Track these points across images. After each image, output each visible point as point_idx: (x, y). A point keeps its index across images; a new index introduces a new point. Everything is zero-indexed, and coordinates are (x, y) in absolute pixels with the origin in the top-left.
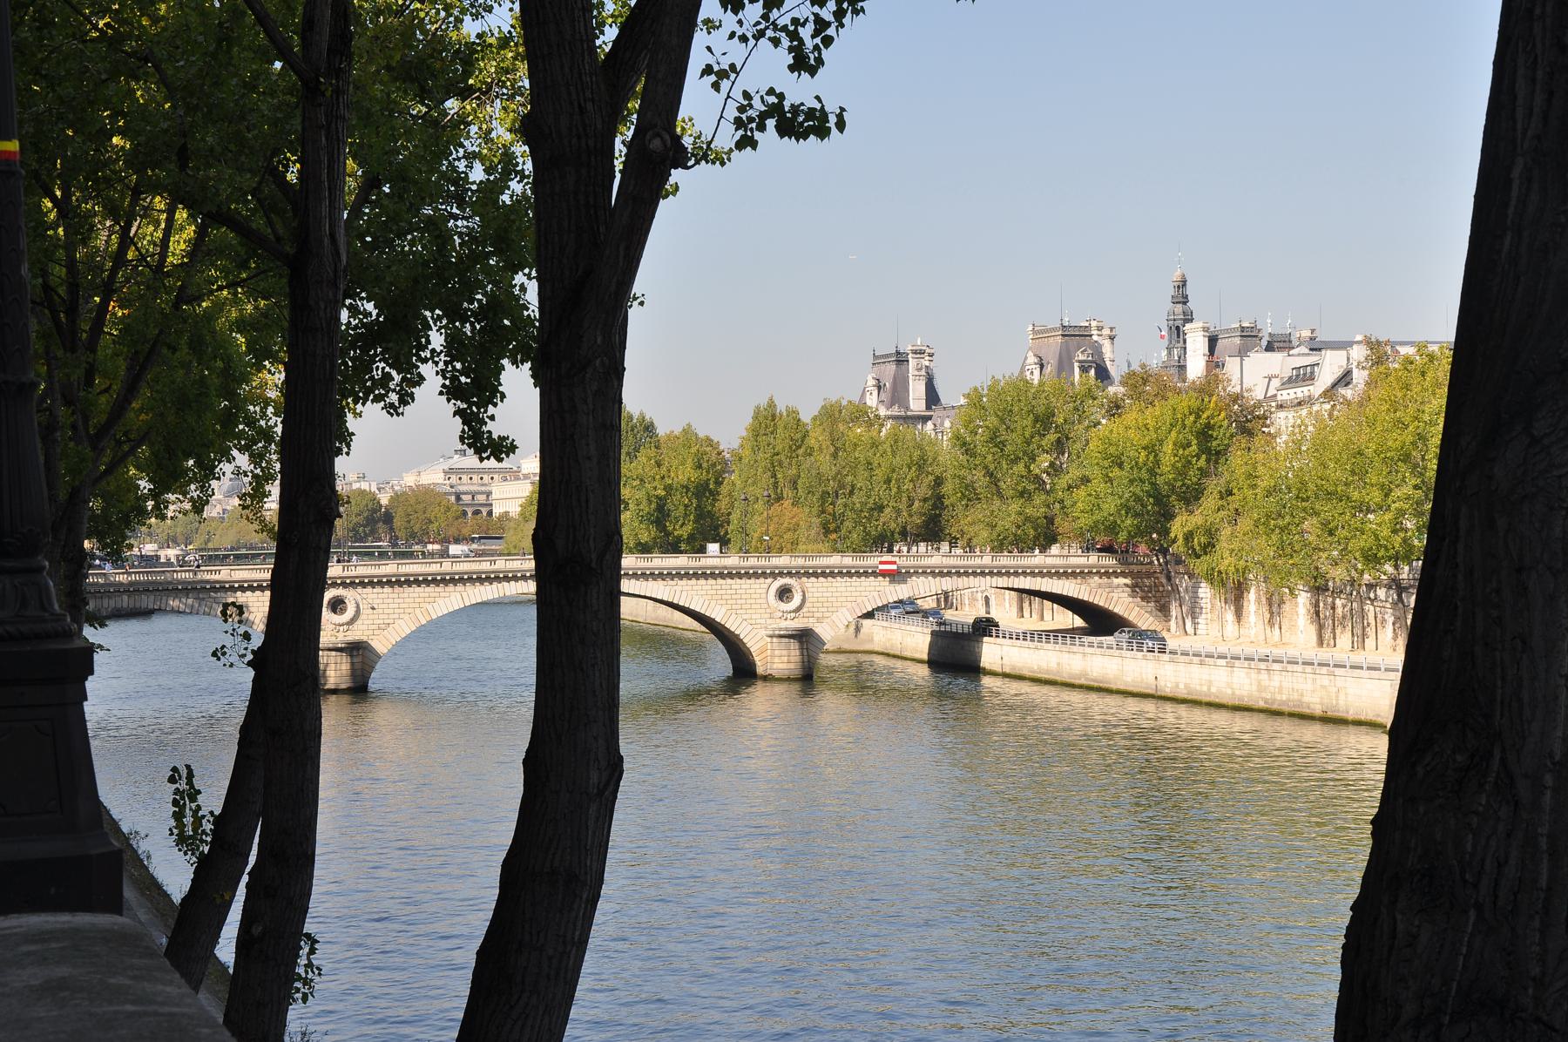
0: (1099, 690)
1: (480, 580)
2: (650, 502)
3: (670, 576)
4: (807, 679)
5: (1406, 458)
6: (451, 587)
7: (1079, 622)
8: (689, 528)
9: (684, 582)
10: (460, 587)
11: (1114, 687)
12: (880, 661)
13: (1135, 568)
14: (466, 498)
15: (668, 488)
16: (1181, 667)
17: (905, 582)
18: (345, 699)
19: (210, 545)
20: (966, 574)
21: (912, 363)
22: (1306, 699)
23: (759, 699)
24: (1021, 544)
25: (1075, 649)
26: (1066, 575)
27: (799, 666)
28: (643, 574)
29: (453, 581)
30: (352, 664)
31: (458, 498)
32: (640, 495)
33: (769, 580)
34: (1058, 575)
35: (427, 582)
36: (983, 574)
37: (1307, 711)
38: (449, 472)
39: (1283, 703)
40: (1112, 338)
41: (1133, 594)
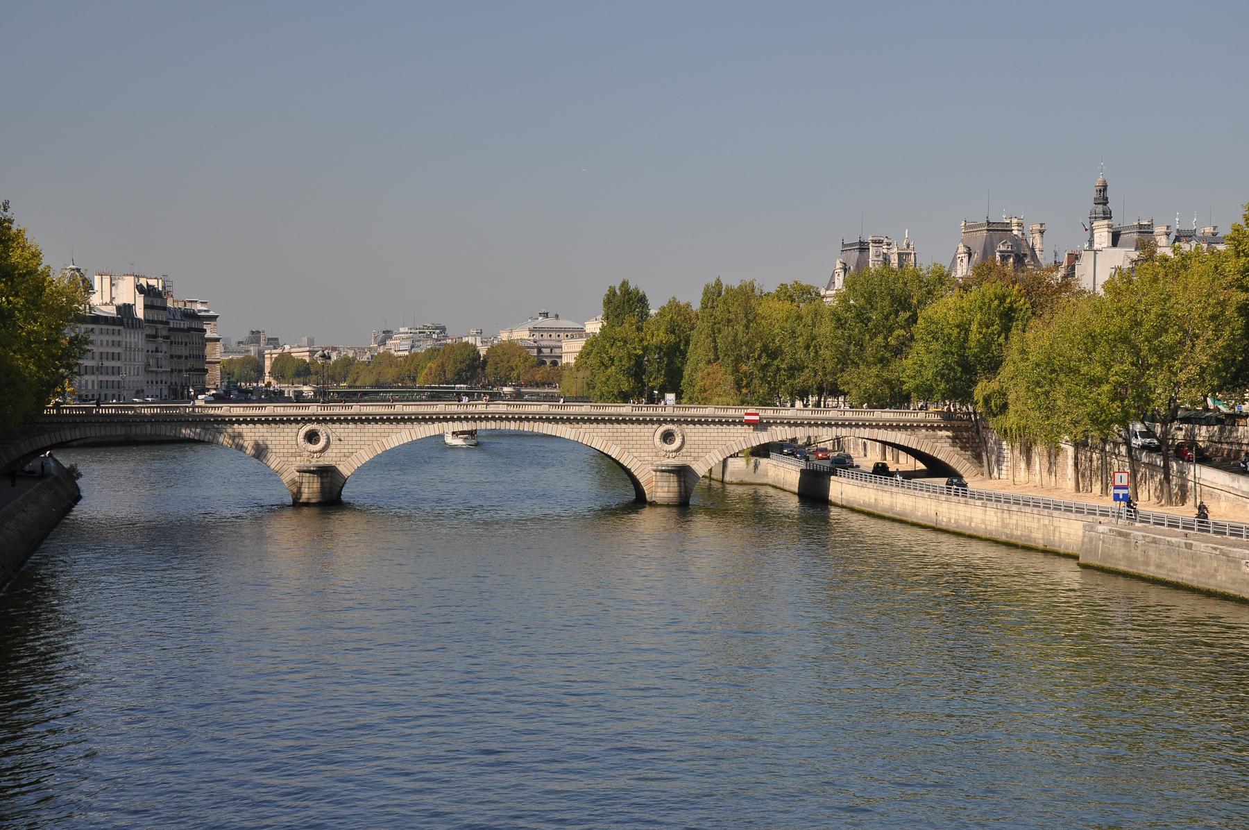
0: (901, 522)
1: (425, 420)
2: (630, 358)
3: (576, 421)
4: (682, 506)
5: (1125, 340)
6: (402, 425)
7: (921, 466)
8: (661, 380)
9: (587, 425)
10: (409, 425)
11: (910, 520)
12: (772, 491)
13: (956, 424)
14: (546, 351)
15: (645, 349)
16: (953, 506)
17: (765, 430)
18: (289, 513)
19: (358, 384)
20: (816, 425)
21: (872, 250)
22: (1033, 535)
23: (648, 521)
24: (879, 403)
25: (886, 488)
26: (898, 427)
27: (676, 495)
28: (554, 419)
29: (403, 420)
30: (322, 483)
31: (540, 351)
32: (623, 353)
33: (656, 426)
34: (892, 427)
35: (382, 421)
36: (830, 425)
37: (1033, 544)
38: (533, 330)
39: (1018, 537)
40: (1042, 232)
41: (954, 444)
